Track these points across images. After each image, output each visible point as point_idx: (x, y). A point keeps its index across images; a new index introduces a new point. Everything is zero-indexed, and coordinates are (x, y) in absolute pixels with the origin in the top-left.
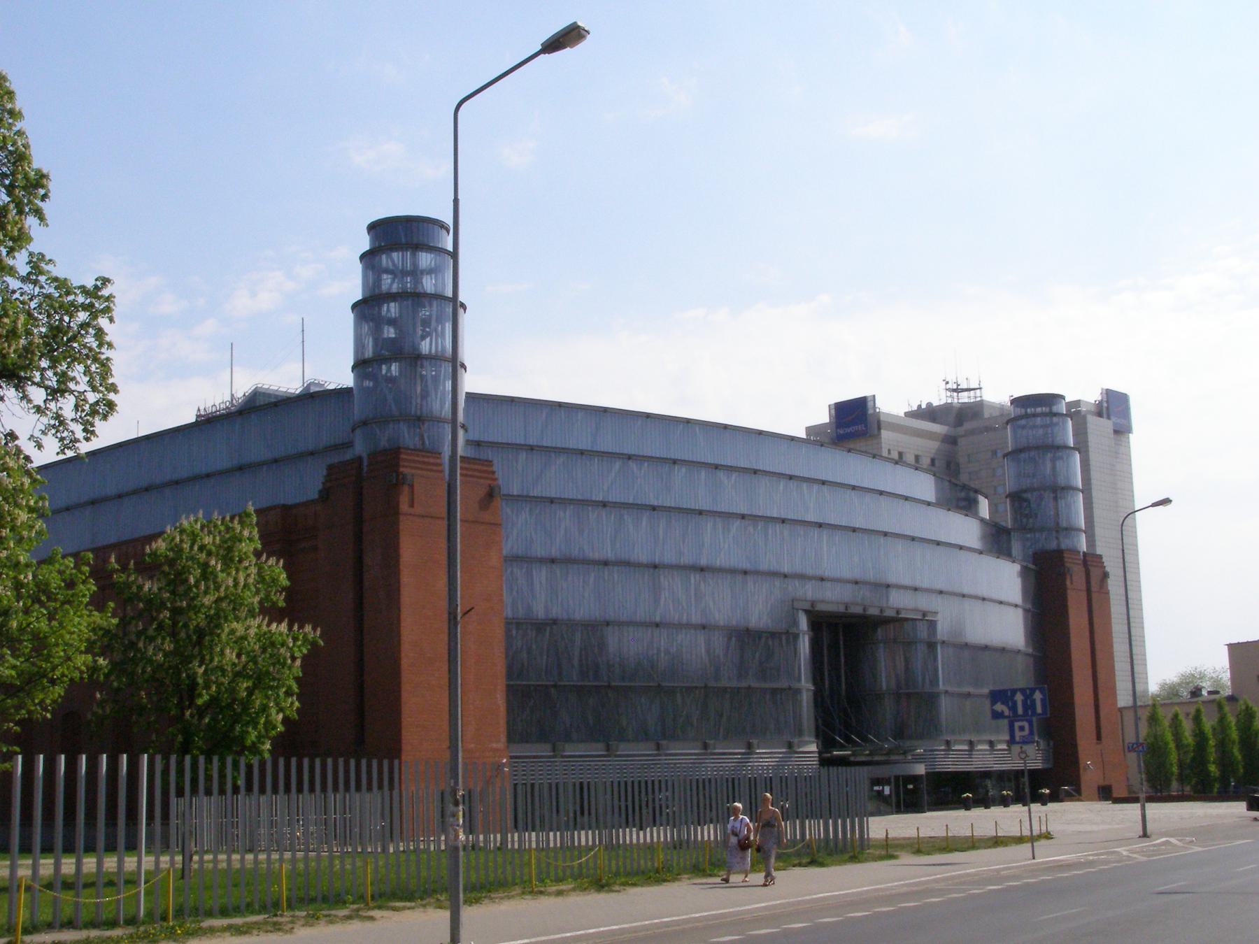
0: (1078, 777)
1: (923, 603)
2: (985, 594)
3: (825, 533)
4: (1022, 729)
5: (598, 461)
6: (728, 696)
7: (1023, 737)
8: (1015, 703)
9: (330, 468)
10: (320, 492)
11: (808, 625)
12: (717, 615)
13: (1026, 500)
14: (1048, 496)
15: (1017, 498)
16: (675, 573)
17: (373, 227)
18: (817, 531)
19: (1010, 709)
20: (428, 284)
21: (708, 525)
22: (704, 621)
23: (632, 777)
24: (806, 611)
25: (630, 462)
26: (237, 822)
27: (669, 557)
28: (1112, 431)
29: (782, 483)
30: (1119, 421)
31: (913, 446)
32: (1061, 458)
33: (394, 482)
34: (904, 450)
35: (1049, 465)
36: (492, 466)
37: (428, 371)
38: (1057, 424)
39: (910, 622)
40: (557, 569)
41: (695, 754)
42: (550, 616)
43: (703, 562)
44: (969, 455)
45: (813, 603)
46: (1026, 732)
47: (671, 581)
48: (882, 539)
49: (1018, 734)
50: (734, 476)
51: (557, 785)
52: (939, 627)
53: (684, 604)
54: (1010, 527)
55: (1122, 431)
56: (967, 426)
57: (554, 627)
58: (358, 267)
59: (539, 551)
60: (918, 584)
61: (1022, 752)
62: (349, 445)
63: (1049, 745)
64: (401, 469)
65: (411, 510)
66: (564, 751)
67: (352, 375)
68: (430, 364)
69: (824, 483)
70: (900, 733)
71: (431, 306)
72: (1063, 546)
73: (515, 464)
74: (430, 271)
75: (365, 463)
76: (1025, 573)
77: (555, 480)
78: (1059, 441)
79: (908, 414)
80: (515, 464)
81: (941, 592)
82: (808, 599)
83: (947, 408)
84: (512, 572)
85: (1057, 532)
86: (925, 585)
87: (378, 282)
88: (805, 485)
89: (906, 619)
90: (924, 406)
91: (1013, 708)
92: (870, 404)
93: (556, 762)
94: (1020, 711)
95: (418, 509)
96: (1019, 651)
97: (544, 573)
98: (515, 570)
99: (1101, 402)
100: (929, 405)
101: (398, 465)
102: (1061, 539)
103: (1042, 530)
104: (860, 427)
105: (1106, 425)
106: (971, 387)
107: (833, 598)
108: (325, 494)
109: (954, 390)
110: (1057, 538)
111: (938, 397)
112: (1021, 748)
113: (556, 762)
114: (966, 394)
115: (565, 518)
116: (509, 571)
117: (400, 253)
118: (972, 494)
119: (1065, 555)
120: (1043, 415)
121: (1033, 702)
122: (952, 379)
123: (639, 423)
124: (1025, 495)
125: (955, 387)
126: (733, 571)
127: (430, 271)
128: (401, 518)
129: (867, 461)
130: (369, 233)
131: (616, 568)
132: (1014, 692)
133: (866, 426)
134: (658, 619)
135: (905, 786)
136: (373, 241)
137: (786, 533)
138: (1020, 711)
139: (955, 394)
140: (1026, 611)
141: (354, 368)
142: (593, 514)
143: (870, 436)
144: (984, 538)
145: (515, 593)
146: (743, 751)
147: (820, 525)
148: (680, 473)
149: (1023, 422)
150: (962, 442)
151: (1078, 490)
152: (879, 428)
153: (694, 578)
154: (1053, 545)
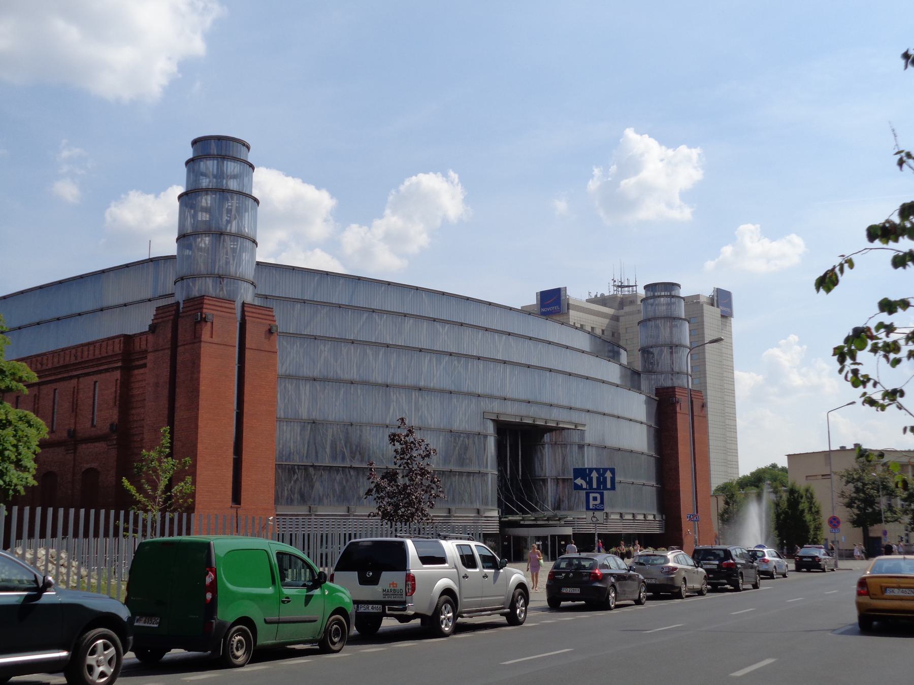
0: (681, 540)
1: (576, 417)
2: (620, 414)
3: (508, 368)
4: (595, 499)
5: (351, 312)
6: (284, 458)
7: (596, 505)
8: (591, 479)
9: (158, 309)
10: (150, 326)
11: (494, 430)
12: (430, 421)
13: (652, 353)
14: (666, 351)
15: (646, 351)
16: (402, 391)
17: (195, 143)
18: (502, 365)
19: (587, 483)
20: (233, 185)
21: (426, 359)
22: (420, 425)
23: (304, 531)
24: (493, 420)
25: (374, 314)
26: (74, 557)
27: (398, 380)
28: (720, 316)
29: (480, 333)
30: (725, 309)
31: (590, 321)
32: (676, 326)
33: (199, 319)
34: (584, 324)
35: (668, 330)
36: (272, 311)
37: (229, 243)
38: (674, 303)
39: (566, 431)
40: (317, 384)
41: (444, 516)
42: (311, 418)
43: (422, 384)
44: (626, 328)
45: (498, 415)
46: (599, 501)
47: (398, 396)
48: (548, 373)
49: (592, 503)
50: (447, 326)
51: (309, 535)
52: (587, 435)
53: (406, 412)
54: (640, 370)
55: (726, 316)
56: (627, 309)
57: (313, 425)
58: (184, 170)
59: (306, 372)
60: (573, 405)
61: (594, 517)
62: (172, 295)
63: (662, 518)
64: (204, 311)
65: (210, 340)
66: (316, 511)
67: (176, 245)
68: (230, 239)
69: (509, 334)
70: (558, 506)
71: (232, 199)
72: (676, 384)
73: (292, 312)
74: (234, 177)
75: (181, 306)
76: (649, 400)
77: (321, 324)
78: (676, 314)
79: (588, 301)
80: (292, 312)
81: (588, 411)
82: (494, 412)
83: (613, 298)
84: (285, 386)
85: (672, 374)
86: (578, 406)
87: (196, 181)
88: (496, 335)
89: (563, 429)
90: (599, 296)
91: (590, 483)
92: (562, 293)
93: (350, 519)
94: (595, 486)
95: (215, 339)
96: (643, 453)
97: (308, 387)
98: (287, 385)
99: (713, 296)
100: (602, 295)
101: (202, 308)
102: (674, 380)
103: (662, 373)
104: (556, 308)
105: (716, 311)
106: (630, 285)
107: (512, 413)
108: (153, 328)
109: (619, 286)
110: (672, 379)
111: (607, 290)
112: (594, 513)
113: (350, 519)
114: (626, 289)
115: (325, 349)
116: (283, 385)
117: (215, 162)
118: (616, 348)
119: (676, 390)
120: (667, 296)
121: (605, 479)
122: (617, 278)
123: (383, 288)
124: (651, 350)
125: (620, 284)
126: (442, 391)
127: (234, 177)
128: (203, 344)
129: (558, 326)
130: (192, 147)
131: (359, 386)
132: (591, 470)
133: (560, 307)
134: (388, 422)
135: (559, 542)
136: (195, 151)
137: (481, 366)
138: (595, 486)
139: (620, 289)
140: (649, 426)
141: (178, 240)
142: (345, 349)
143: (562, 314)
144: (623, 377)
145: (286, 400)
146: (445, 515)
147: (505, 362)
148: (409, 323)
149: (651, 301)
150: (621, 319)
151: (686, 347)
152: (568, 309)
153: (414, 394)
154: (668, 384)
